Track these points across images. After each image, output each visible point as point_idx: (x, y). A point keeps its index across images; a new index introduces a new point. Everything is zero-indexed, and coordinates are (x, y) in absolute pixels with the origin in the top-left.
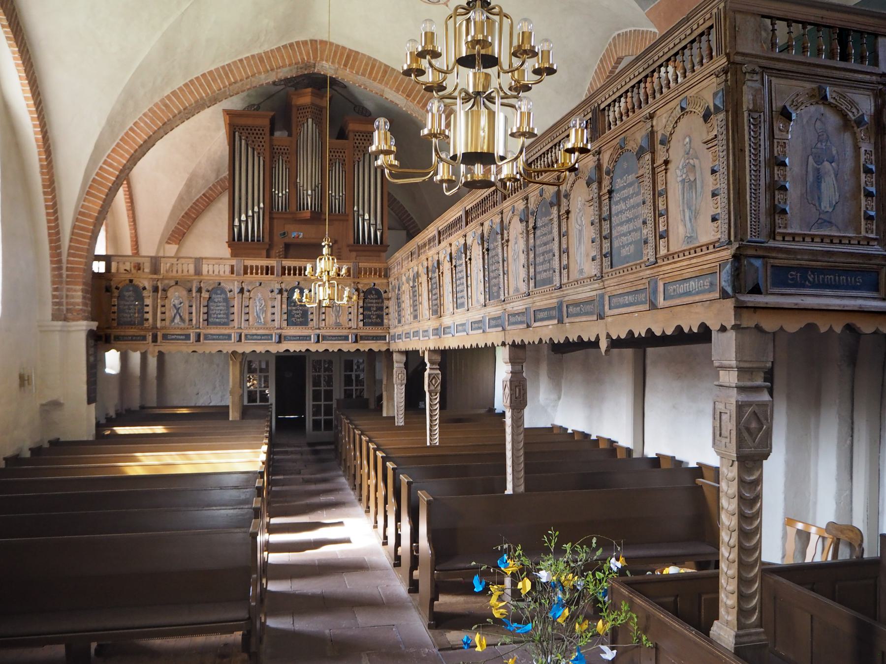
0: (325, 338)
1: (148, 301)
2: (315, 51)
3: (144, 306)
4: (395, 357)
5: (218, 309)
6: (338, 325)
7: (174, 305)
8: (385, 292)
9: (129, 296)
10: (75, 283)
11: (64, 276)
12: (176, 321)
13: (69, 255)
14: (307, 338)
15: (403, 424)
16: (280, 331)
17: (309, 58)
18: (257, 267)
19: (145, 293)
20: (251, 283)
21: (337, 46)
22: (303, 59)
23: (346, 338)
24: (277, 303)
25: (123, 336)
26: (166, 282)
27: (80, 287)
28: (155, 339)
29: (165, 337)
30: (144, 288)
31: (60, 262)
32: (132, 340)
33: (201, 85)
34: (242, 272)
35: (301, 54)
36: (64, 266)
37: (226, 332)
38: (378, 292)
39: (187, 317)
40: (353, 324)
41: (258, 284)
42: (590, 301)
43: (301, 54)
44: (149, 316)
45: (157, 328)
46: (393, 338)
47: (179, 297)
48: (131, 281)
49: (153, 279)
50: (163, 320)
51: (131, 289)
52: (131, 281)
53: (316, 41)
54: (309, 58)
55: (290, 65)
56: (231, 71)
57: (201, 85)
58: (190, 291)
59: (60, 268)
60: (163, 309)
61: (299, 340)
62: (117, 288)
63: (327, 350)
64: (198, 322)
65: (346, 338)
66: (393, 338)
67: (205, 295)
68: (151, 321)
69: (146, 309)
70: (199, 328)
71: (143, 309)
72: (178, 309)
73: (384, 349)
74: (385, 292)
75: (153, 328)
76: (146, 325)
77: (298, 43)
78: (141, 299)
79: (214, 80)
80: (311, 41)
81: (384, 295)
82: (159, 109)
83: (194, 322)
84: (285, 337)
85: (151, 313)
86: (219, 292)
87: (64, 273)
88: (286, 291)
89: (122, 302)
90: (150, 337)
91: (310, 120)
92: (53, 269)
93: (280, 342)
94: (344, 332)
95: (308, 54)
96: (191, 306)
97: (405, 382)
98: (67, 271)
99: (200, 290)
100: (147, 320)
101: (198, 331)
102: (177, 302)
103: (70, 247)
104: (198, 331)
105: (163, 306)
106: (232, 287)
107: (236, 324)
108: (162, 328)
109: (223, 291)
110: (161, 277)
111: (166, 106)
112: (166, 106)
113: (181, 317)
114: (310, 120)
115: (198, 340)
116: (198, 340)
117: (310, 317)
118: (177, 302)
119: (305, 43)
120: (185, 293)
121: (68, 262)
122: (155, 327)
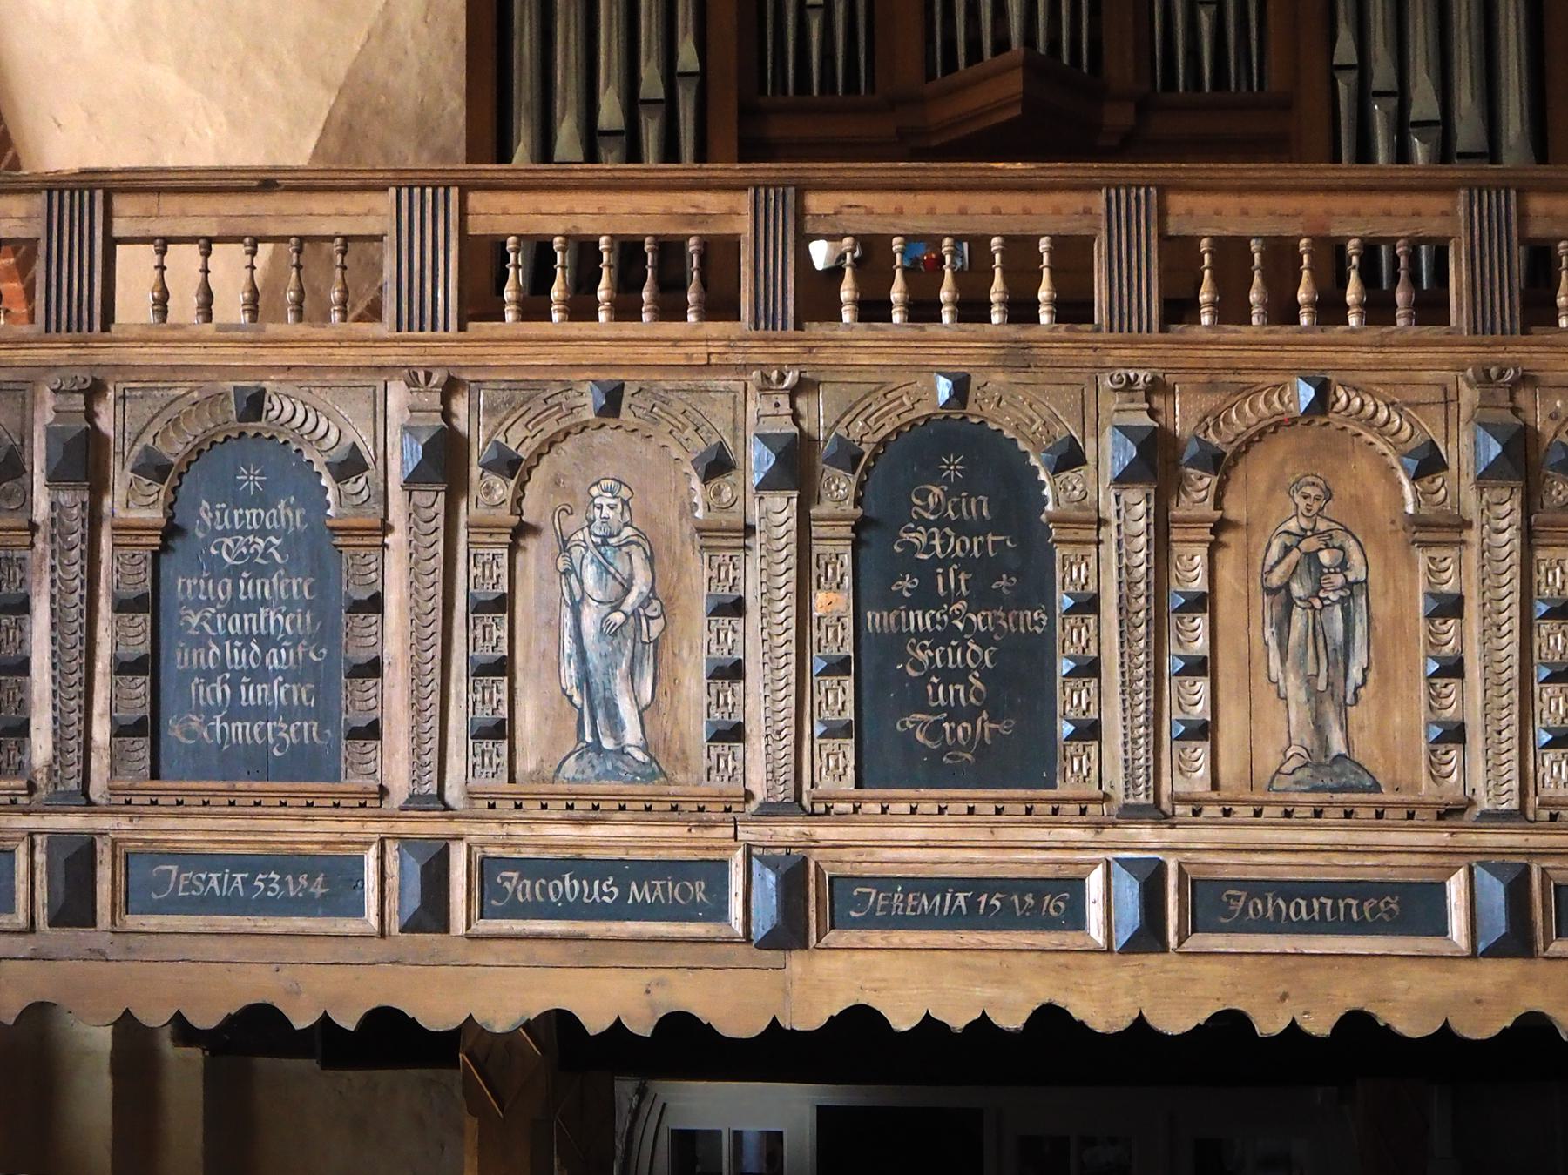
0: (1214, 903)
5: (244, 632)
6: (1337, 781)
14: (1049, 902)
16: (788, 832)
18: (585, 249)
23: (1416, 907)
34: (449, 295)
41: (588, 402)
61: (971, 919)
67: (131, 503)
70: (83, 800)
76: (1079, 771)
88: (848, 456)
93: (789, 934)
94: (1400, 848)
107: (397, 766)
115: (431, 913)
117: (1072, 702)
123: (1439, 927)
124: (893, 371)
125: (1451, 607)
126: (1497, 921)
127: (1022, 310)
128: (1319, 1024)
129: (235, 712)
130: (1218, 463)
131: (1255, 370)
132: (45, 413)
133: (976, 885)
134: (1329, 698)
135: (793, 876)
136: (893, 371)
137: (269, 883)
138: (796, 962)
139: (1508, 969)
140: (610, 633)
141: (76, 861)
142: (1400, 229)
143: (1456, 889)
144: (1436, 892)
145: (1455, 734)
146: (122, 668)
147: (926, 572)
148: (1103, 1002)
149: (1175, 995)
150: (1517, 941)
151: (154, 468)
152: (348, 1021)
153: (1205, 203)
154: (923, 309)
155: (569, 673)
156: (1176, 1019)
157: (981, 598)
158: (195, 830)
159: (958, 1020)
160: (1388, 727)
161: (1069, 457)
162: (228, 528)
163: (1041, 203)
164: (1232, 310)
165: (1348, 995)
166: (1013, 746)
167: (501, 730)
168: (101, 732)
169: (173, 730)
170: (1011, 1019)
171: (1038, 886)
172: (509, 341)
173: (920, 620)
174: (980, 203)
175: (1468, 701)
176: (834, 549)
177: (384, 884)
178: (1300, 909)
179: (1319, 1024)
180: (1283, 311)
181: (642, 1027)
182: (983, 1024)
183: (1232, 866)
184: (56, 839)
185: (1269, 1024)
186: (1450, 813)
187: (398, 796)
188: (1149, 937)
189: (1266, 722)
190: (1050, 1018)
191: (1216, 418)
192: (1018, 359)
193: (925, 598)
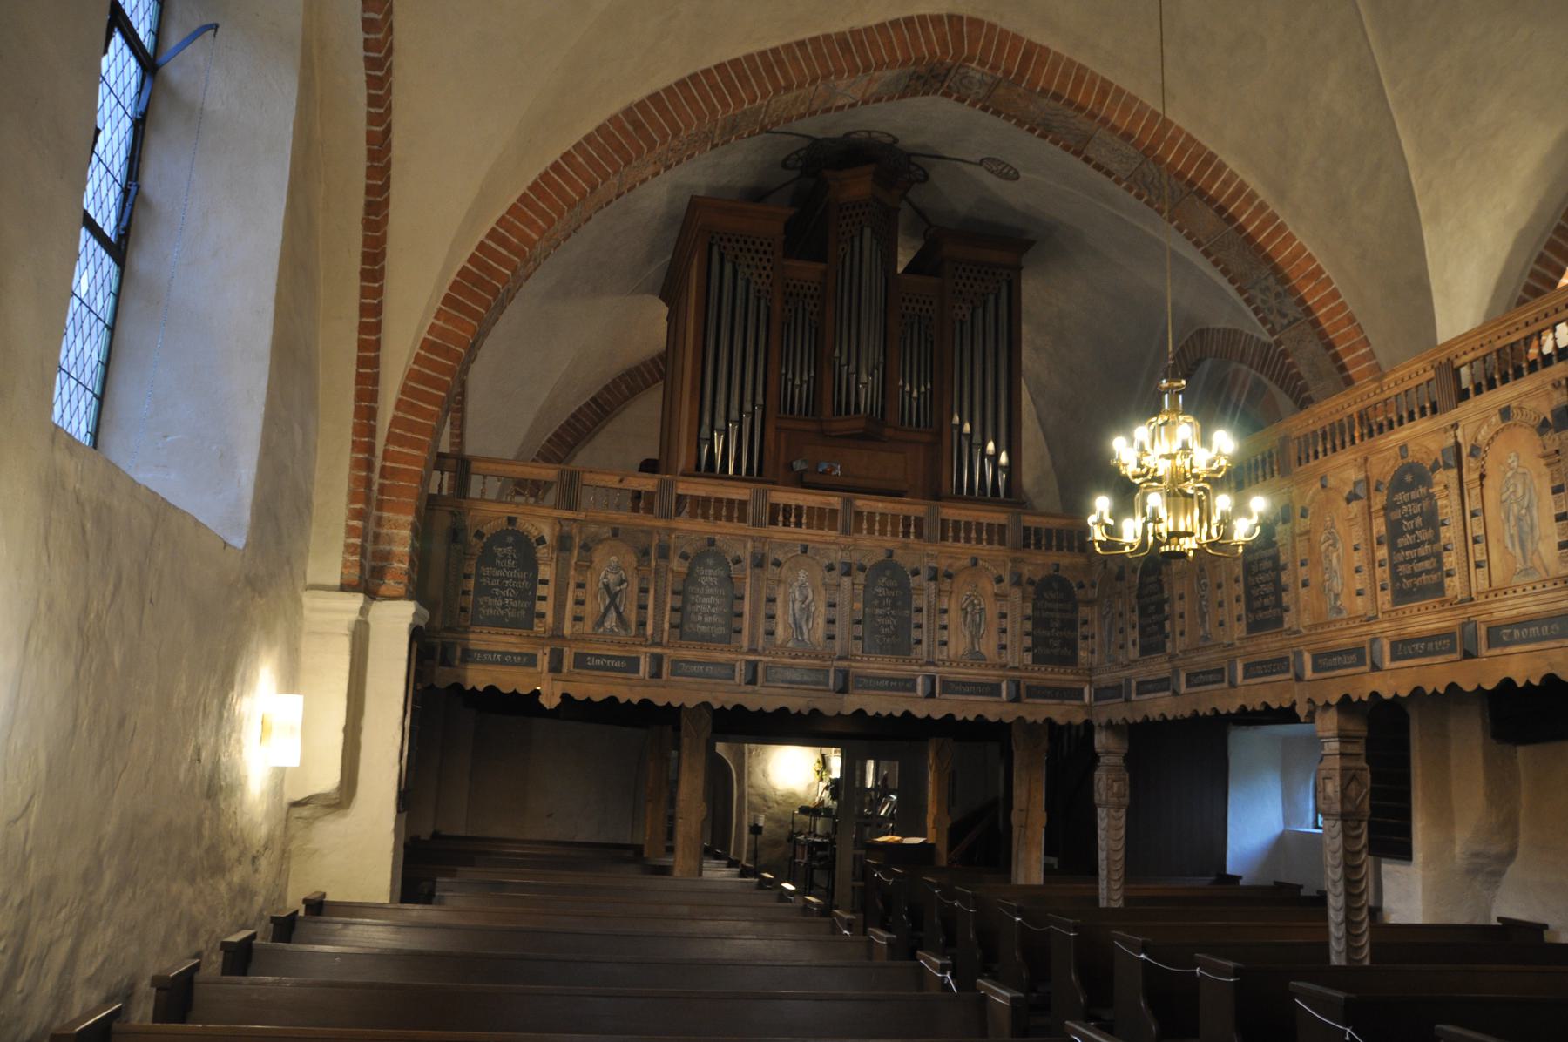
0: (948, 687)
1: (546, 572)
2: (958, 37)
3: (535, 581)
4: (1101, 740)
5: (708, 605)
6: (976, 657)
7: (606, 586)
8: (1081, 586)
9: (505, 557)
10: (398, 508)
11: (375, 487)
12: (607, 624)
13: (391, 438)
14: (907, 684)
15: (1120, 904)
16: (845, 664)
17: (945, 52)
18: (799, 508)
19: (542, 552)
20: (783, 545)
21: (1004, 33)
22: (932, 53)
23: (994, 690)
24: (843, 598)
25: (482, 652)
26: (593, 528)
27: (410, 518)
28: (555, 667)
29: (581, 661)
30: (541, 541)
31: (371, 449)
32: (503, 663)
33: (715, 87)
34: (766, 518)
35: (928, 41)
36: (378, 463)
37: (722, 657)
38: (1064, 586)
39: (632, 617)
40: (1008, 658)
41: (799, 550)
42: (1448, 635)
43: (928, 41)
44: (546, 607)
45: (563, 637)
46: (467, 656)
47: (618, 567)
48: (512, 521)
49: (559, 520)
50: (577, 619)
51: (510, 539)
52: (512, 521)
53: (960, 18)
54: (945, 52)
55: (904, 63)
56: (780, 62)
57: (715, 87)
58: (645, 553)
59: (369, 466)
60: (580, 593)
61: (889, 688)
62: (479, 535)
63: (950, 717)
64: (658, 627)
65: (994, 690)
66: (467, 656)
67: (677, 565)
68: (549, 619)
69: (542, 590)
70: (660, 644)
71: (534, 589)
72: (613, 596)
73: (1079, 719)
74: (1081, 586)
75: (553, 637)
76: (539, 627)
77: (922, 18)
78: (530, 564)
79: (744, 79)
80: (951, 17)
81: (1079, 594)
82: (622, 129)
83: (650, 629)
84: (857, 677)
85: (551, 600)
86: (710, 562)
87: (376, 478)
88: (862, 568)
89: (486, 570)
90: (546, 659)
91: (867, 232)
92: (356, 464)
93: (843, 690)
94: (991, 675)
95: (944, 45)
96: (645, 591)
97: (1126, 800)
98: (382, 476)
99: (664, 553)
100: (543, 615)
101: (658, 650)
102: (612, 578)
103: (395, 422)
104: (658, 650)
105: (580, 586)
106: (740, 553)
107: (745, 640)
108: (576, 639)
109: (720, 560)
110: (582, 516)
111: (638, 125)
112: (638, 125)
113: (619, 614)
114: (867, 232)
115: (656, 674)
116: (656, 674)
117: (915, 634)
118: (612, 578)
119: (937, 20)
120: (631, 559)
121: (387, 455)
122: (557, 634)
123: (999, 695)
124: (870, 546)
125: (1003, 616)
126: (840, 685)
127: (906, 534)
128: (635, 701)
129: (703, 624)
130: (950, 576)
131: (958, 552)
132: (655, 541)
133: (891, 679)
134: (975, 637)
135: (845, 674)
136: (870, 546)
137: (709, 669)
138: (846, 697)
139: (1015, 705)
140: (802, 609)
141: (657, 661)
142: (996, 522)
143: (1004, 686)
144: (998, 686)
145: (1004, 647)
146: (673, 609)
147: (881, 599)
148: (920, 711)
149: (936, 709)
150: (1016, 699)
151: (684, 556)
152: (729, 707)
153: (951, 511)
154: (883, 532)
155: (791, 620)
156: (937, 715)
157: (894, 606)
158: (688, 654)
159: (884, 713)
160: (988, 646)
161: (916, 573)
162: (709, 575)
163: (913, 508)
164: (956, 539)
165: (979, 711)
166: (1067, 658)
167: (771, 633)
168: (666, 626)
169: (686, 627)
170: (898, 714)
171: (907, 680)
172: (779, 532)
173: (879, 611)
174: (898, 507)
175: (1007, 639)
176: (860, 590)
177: (740, 670)
178: (968, 689)
179: (971, 718)
180: (968, 540)
181: (806, 712)
182: (891, 715)
183: (952, 677)
184: (653, 655)
185: (959, 717)
186: (1003, 666)
187: (745, 649)
188: (931, 695)
189: (958, 644)
190: (907, 714)
191: (950, 566)
192: (906, 547)
193: (880, 606)
